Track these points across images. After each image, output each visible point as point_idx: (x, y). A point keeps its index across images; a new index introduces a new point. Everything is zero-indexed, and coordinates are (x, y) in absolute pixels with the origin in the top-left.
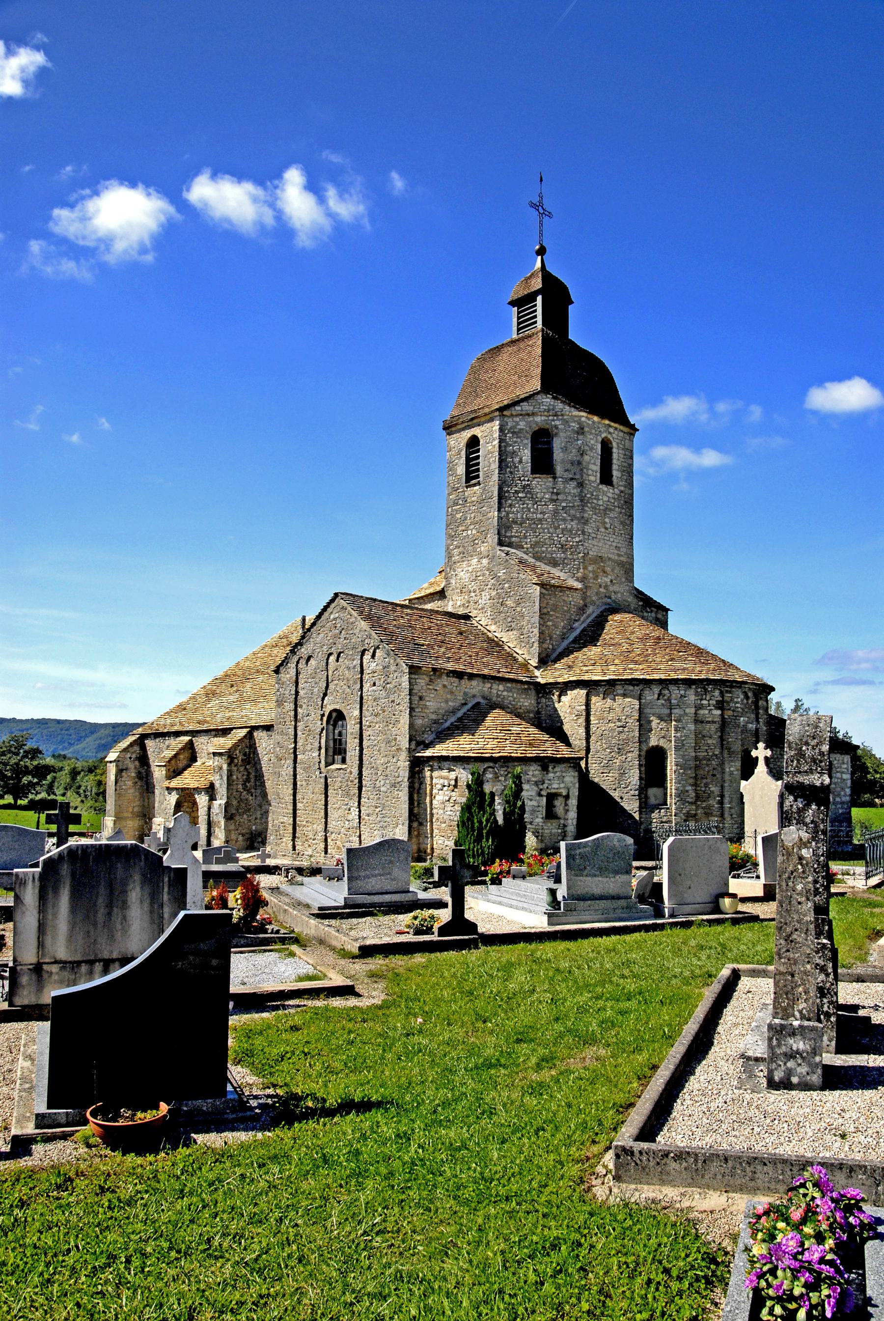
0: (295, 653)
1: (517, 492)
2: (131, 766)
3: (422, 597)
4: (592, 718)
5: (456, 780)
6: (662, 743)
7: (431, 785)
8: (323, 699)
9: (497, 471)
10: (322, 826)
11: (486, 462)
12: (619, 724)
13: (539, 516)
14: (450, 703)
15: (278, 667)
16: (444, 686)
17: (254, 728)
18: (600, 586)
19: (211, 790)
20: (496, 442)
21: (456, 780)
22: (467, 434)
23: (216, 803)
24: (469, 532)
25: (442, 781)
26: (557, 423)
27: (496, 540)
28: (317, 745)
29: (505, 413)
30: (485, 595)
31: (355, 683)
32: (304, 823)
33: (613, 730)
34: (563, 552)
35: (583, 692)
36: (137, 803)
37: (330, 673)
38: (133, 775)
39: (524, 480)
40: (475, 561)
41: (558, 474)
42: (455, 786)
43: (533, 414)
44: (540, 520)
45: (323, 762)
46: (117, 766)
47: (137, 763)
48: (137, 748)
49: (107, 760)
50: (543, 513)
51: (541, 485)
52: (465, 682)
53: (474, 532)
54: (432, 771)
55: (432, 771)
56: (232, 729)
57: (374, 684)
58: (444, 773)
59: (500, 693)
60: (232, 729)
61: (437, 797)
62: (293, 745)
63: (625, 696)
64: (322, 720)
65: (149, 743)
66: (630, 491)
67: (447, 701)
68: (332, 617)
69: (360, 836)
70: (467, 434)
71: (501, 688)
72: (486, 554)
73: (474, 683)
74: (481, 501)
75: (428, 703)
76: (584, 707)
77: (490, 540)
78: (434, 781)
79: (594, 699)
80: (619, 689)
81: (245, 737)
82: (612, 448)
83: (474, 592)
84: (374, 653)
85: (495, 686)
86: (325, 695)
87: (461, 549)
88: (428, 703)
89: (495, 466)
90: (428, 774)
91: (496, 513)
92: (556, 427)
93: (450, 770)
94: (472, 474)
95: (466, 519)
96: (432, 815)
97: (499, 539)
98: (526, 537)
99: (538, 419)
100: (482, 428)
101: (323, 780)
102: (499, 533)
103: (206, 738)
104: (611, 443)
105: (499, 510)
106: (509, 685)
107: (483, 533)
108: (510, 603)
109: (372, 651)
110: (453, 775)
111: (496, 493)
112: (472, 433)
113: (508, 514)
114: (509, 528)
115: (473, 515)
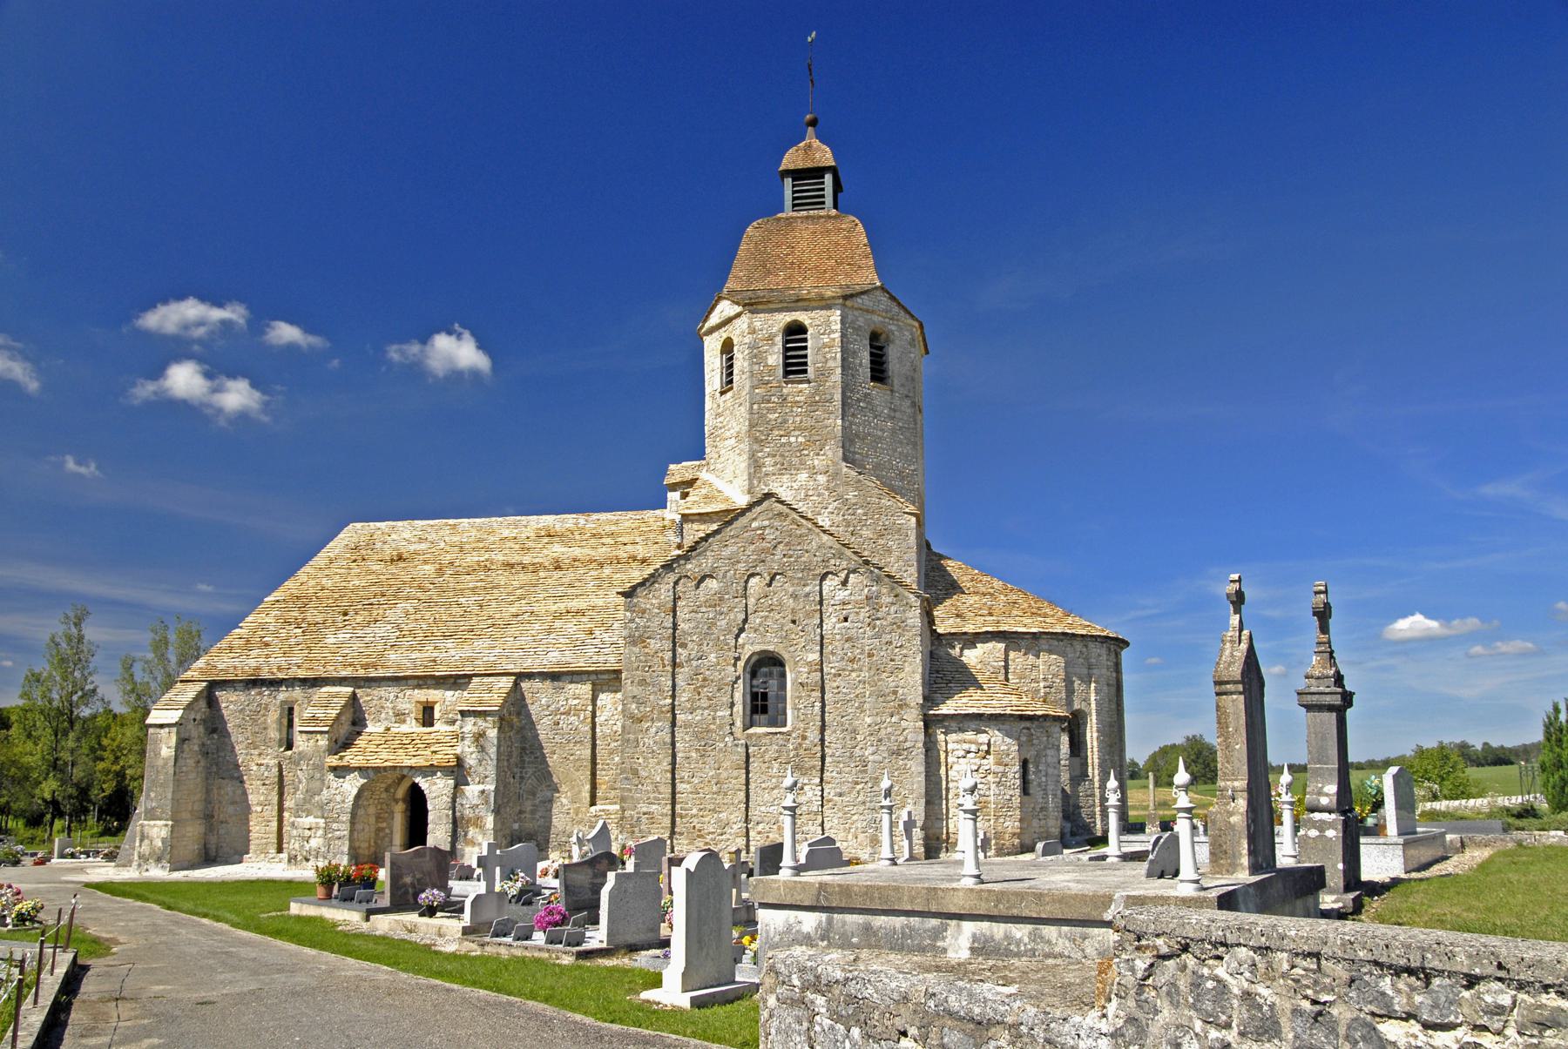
0: (673, 570)
1: (859, 400)
2: (194, 733)
3: (707, 514)
5: (989, 745)
6: (1083, 706)
7: (946, 752)
8: (737, 636)
9: (839, 370)
10: (742, 816)
11: (820, 358)
15: (634, 588)
17: (521, 676)
19: (458, 772)
20: (837, 335)
21: (989, 745)
22: (788, 317)
23: (472, 791)
24: (793, 439)
25: (966, 746)
27: (840, 454)
28: (726, 699)
29: (848, 303)
31: (808, 615)
32: (694, 811)
35: (1002, 646)
36: (198, 796)
37: (752, 601)
38: (196, 748)
40: (803, 476)
41: (896, 388)
42: (988, 752)
43: (873, 312)
45: (739, 723)
46: (178, 733)
47: (201, 728)
48: (203, 704)
49: (149, 721)
51: (876, 391)
54: (946, 734)
55: (946, 734)
56: (470, 677)
57: (846, 620)
58: (969, 735)
60: (470, 677)
61: (955, 767)
62: (669, 701)
63: (1050, 652)
64: (735, 665)
65: (229, 701)
68: (754, 525)
69: (822, 824)
70: (788, 317)
72: (823, 469)
74: (812, 404)
77: (830, 453)
78: (950, 747)
79: (1012, 655)
80: (1043, 643)
81: (196, 699)
84: (847, 577)
86: (742, 630)
87: (778, 459)
90: (941, 737)
91: (839, 422)
93: (979, 732)
94: (794, 365)
95: (785, 421)
96: (948, 789)
99: (876, 318)
100: (813, 314)
101: (741, 750)
103: (396, 689)
109: (843, 575)
110: (983, 738)
111: (838, 397)
114: (852, 442)
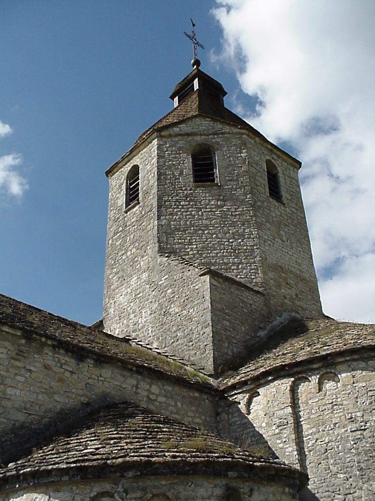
4: (305, 427)
12: (354, 426)
13: (207, 222)
14: (57, 397)
16: (47, 367)
18: (285, 298)
26: (218, 140)
29: (163, 133)
30: (146, 312)
33: (344, 439)
34: (237, 257)
39: (186, 190)
44: (207, 226)
50: (210, 219)
52: (88, 367)
53: (134, 250)
59: (153, 397)
66: (287, 471)
67: (50, 393)
71: (155, 389)
73: (107, 372)
75: (9, 391)
76: (290, 410)
82: (277, 174)
83: (133, 313)
85: (144, 385)
88: (9, 391)
89: (154, 181)
92: (218, 143)
94: (132, 196)
97: (160, 246)
98: (190, 244)
102: (159, 241)
104: (276, 168)
105: (159, 219)
106: (169, 388)
107: (142, 248)
108: (174, 309)
111: (155, 204)
112: (132, 165)
113: (169, 221)
115: (132, 236)
